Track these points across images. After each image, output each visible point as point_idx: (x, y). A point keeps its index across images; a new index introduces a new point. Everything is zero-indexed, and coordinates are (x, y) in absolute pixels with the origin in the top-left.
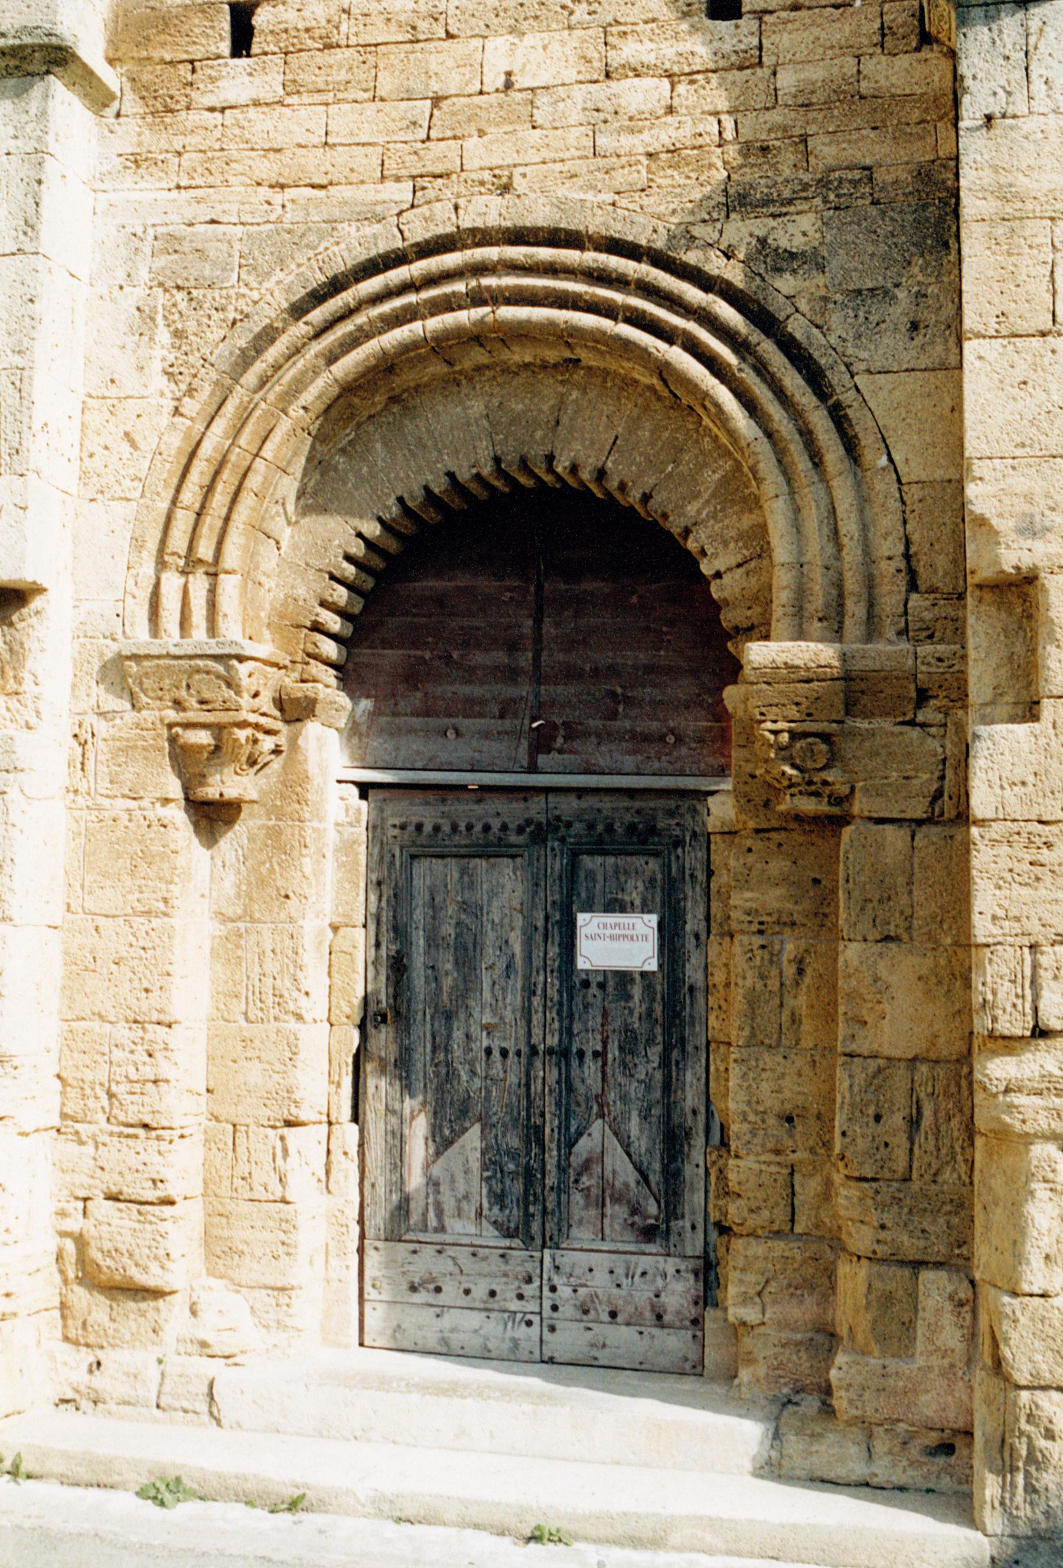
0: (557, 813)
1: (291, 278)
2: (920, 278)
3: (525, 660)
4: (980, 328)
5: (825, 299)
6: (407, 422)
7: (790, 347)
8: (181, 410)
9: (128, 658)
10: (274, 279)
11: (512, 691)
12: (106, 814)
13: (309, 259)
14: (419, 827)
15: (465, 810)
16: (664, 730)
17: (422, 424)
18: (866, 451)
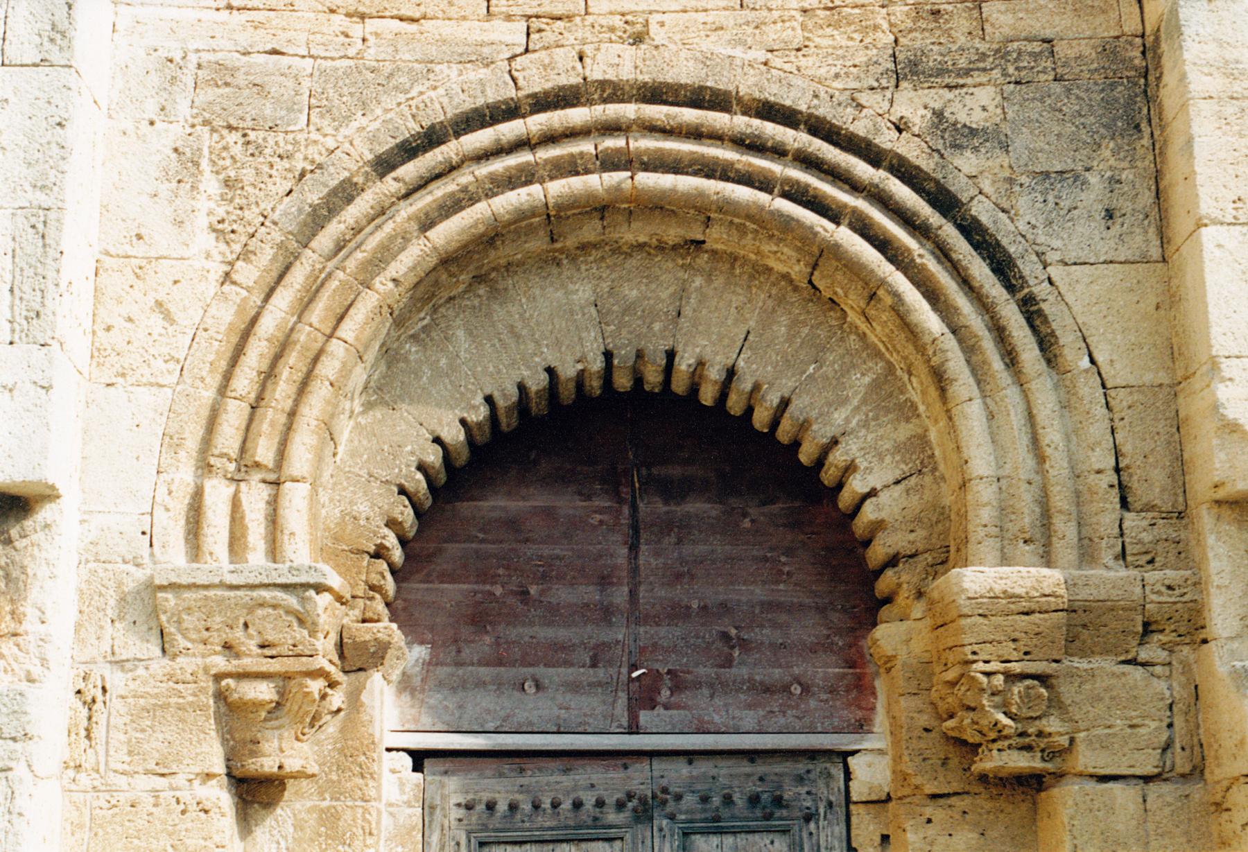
0: (664, 782)
1: (377, 125)
2: (1112, 162)
3: (620, 596)
4: (1216, 214)
5: (1011, 181)
6: (496, 307)
7: (972, 231)
8: (235, 277)
9: (162, 588)
10: (354, 125)
11: (605, 635)
12: (122, 797)
13: (399, 104)
14: (491, 806)
15: (552, 783)
16: (788, 679)
17: (514, 309)
18: (1066, 351)
